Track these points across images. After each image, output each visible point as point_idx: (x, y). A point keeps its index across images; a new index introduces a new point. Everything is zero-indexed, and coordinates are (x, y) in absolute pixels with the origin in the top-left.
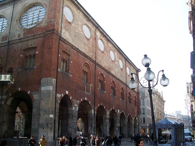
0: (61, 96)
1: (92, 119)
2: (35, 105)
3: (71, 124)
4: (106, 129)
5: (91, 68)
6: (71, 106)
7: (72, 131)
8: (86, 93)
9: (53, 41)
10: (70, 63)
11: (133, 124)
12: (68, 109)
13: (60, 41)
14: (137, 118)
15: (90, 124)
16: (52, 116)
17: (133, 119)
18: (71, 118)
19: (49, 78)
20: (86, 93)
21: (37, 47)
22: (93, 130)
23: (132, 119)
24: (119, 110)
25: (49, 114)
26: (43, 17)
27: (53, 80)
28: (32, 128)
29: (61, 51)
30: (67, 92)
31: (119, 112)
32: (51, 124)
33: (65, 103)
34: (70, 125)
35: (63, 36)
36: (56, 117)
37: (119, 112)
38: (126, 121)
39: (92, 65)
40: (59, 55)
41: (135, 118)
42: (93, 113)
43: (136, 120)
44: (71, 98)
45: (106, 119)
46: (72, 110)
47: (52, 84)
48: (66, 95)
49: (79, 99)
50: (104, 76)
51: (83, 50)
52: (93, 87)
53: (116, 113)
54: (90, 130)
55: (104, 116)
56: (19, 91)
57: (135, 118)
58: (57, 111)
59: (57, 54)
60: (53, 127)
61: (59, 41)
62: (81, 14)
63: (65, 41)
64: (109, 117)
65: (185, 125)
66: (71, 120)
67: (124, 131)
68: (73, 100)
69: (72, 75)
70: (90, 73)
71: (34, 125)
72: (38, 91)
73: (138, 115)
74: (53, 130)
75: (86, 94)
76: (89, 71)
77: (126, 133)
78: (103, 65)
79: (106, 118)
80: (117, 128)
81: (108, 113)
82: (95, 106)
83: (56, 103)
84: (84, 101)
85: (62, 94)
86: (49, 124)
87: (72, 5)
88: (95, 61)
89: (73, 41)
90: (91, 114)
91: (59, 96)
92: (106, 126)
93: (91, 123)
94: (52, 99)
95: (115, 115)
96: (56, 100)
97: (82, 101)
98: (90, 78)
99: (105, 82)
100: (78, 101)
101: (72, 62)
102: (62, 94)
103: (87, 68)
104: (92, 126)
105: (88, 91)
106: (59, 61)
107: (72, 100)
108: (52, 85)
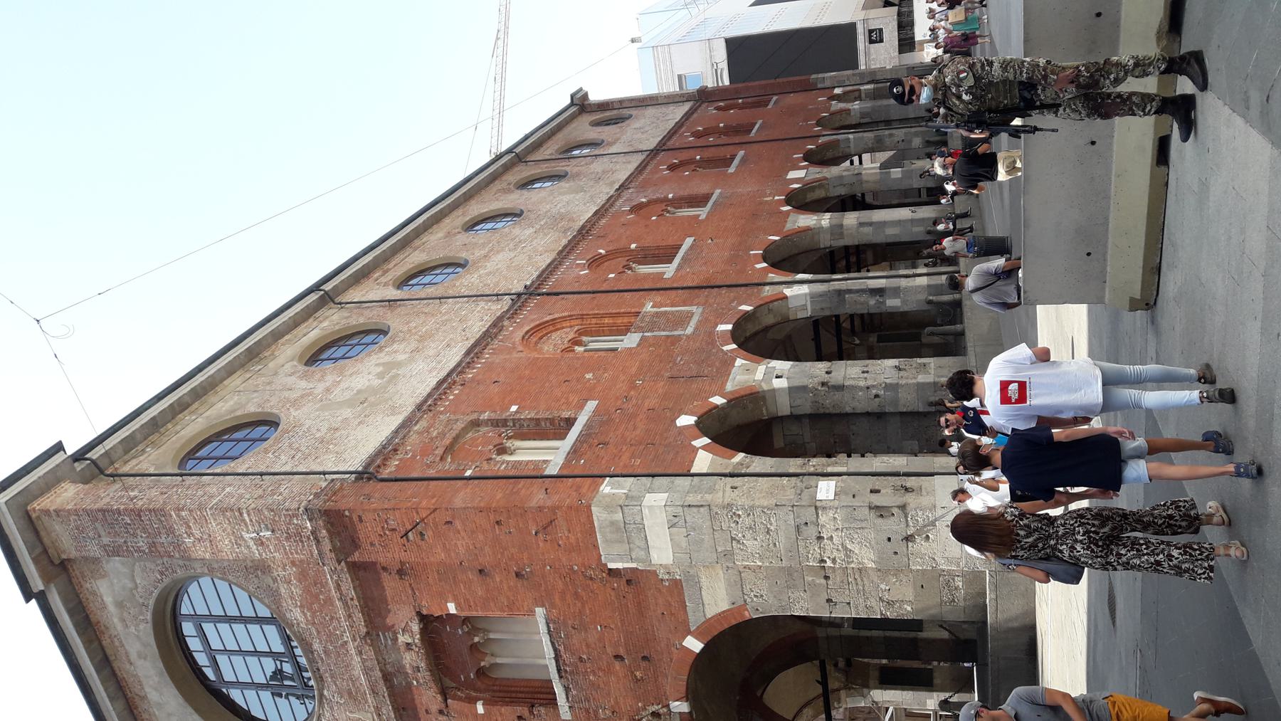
0: (704, 448)
1: (840, 293)
2: (766, 601)
3: (874, 392)
4: (899, 223)
5: (556, 316)
6: (764, 398)
7: (918, 384)
8: (690, 330)
9: (375, 510)
10: (518, 416)
11: (868, 105)
12: (782, 419)
13: (385, 473)
14: (837, 91)
15: (872, 302)
16: (826, 490)
17: (836, 106)
18: (838, 395)
19: (598, 514)
20: (690, 330)
21: (419, 614)
22: (904, 283)
23: (841, 111)
24: (793, 175)
25: (817, 507)
26: (242, 596)
27: (608, 495)
28: (907, 611)
29: (449, 466)
30: (686, 420)
31: (800, 174)
32: (878, 491)
33: (750, 430)
34: (877, 396)
35: (355, 461)
36: (830, 470)
37: (800, 174)
38: (851, 136)
39: (532, 315)
40: (468, 473)
41: (839, 98)
42: (804, 289)
43: (845, 93)
44: (718, 400)
45: (842, 226)
46: (792, 390)
47: (633, 500)
48: (703, 426)
49: (728, 362)
50: (602, 251)
51: (453, 357)
52: (658, 299)
53: (808, 187)
54: (904, 302)
55: (826, 242)
56: (692, 707)
57: (839, 98)
58: (793, 465)
59: (460, 483)
60: (898, 481)
61: (383, 480)
62: (235, 381)
63: (385, 452)
64: (828, 215)
65: (1129, 445)
66: (847, 396)
67: (910, 142)
68: (729, 387)
69: (587, 400)
70: (582, 317)
71: (890, 603)
72: (677, 584)
73: (820, 86)
74: (910, 482)
75: (696, 329)
76: (573, 322)
77: (916, 134)
78: (544, 261)
79: (837, 229)
80: (893, 176)
81: (806, 220)
82: (765, 284)
83: (748, 471)
84: (735, 336)
85: (694, 443)
86: (877, 500)
87: (178, 427)
88: (519, 295)
89: (393, 411)
90: (813, 296)
91: (703, 461)
92: (884, 224)
93: (864, 298)
94: (723, 492)
95: (769, 320)
96: (732, 475)
97: (734, 346)
98: (612, 315)
99: (633, 246)
100: (739, 362)
101: (514, 408)
102: (694, 443)
103: (554, 335)
104: (879, 292)
105: (683, 320)
106: (500, 474)
107: (731, 392)
108: (640, 499)
